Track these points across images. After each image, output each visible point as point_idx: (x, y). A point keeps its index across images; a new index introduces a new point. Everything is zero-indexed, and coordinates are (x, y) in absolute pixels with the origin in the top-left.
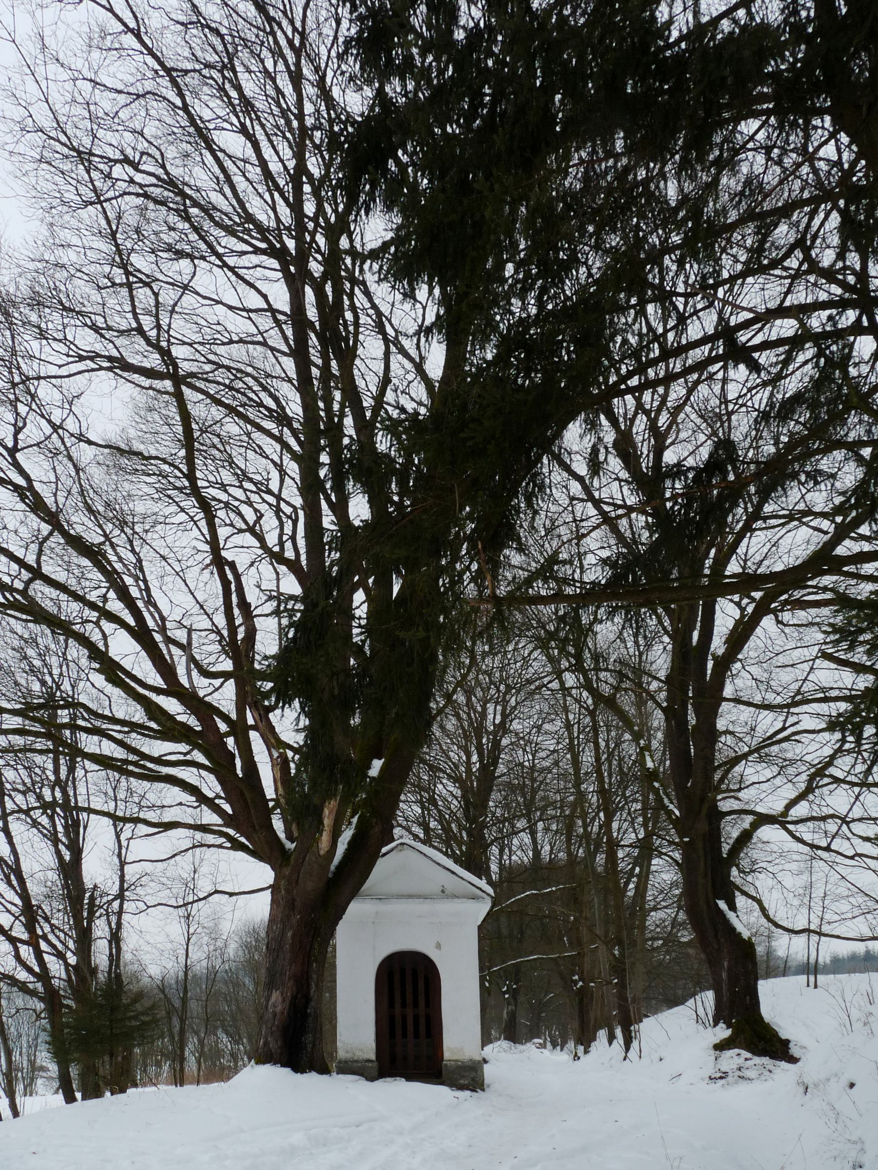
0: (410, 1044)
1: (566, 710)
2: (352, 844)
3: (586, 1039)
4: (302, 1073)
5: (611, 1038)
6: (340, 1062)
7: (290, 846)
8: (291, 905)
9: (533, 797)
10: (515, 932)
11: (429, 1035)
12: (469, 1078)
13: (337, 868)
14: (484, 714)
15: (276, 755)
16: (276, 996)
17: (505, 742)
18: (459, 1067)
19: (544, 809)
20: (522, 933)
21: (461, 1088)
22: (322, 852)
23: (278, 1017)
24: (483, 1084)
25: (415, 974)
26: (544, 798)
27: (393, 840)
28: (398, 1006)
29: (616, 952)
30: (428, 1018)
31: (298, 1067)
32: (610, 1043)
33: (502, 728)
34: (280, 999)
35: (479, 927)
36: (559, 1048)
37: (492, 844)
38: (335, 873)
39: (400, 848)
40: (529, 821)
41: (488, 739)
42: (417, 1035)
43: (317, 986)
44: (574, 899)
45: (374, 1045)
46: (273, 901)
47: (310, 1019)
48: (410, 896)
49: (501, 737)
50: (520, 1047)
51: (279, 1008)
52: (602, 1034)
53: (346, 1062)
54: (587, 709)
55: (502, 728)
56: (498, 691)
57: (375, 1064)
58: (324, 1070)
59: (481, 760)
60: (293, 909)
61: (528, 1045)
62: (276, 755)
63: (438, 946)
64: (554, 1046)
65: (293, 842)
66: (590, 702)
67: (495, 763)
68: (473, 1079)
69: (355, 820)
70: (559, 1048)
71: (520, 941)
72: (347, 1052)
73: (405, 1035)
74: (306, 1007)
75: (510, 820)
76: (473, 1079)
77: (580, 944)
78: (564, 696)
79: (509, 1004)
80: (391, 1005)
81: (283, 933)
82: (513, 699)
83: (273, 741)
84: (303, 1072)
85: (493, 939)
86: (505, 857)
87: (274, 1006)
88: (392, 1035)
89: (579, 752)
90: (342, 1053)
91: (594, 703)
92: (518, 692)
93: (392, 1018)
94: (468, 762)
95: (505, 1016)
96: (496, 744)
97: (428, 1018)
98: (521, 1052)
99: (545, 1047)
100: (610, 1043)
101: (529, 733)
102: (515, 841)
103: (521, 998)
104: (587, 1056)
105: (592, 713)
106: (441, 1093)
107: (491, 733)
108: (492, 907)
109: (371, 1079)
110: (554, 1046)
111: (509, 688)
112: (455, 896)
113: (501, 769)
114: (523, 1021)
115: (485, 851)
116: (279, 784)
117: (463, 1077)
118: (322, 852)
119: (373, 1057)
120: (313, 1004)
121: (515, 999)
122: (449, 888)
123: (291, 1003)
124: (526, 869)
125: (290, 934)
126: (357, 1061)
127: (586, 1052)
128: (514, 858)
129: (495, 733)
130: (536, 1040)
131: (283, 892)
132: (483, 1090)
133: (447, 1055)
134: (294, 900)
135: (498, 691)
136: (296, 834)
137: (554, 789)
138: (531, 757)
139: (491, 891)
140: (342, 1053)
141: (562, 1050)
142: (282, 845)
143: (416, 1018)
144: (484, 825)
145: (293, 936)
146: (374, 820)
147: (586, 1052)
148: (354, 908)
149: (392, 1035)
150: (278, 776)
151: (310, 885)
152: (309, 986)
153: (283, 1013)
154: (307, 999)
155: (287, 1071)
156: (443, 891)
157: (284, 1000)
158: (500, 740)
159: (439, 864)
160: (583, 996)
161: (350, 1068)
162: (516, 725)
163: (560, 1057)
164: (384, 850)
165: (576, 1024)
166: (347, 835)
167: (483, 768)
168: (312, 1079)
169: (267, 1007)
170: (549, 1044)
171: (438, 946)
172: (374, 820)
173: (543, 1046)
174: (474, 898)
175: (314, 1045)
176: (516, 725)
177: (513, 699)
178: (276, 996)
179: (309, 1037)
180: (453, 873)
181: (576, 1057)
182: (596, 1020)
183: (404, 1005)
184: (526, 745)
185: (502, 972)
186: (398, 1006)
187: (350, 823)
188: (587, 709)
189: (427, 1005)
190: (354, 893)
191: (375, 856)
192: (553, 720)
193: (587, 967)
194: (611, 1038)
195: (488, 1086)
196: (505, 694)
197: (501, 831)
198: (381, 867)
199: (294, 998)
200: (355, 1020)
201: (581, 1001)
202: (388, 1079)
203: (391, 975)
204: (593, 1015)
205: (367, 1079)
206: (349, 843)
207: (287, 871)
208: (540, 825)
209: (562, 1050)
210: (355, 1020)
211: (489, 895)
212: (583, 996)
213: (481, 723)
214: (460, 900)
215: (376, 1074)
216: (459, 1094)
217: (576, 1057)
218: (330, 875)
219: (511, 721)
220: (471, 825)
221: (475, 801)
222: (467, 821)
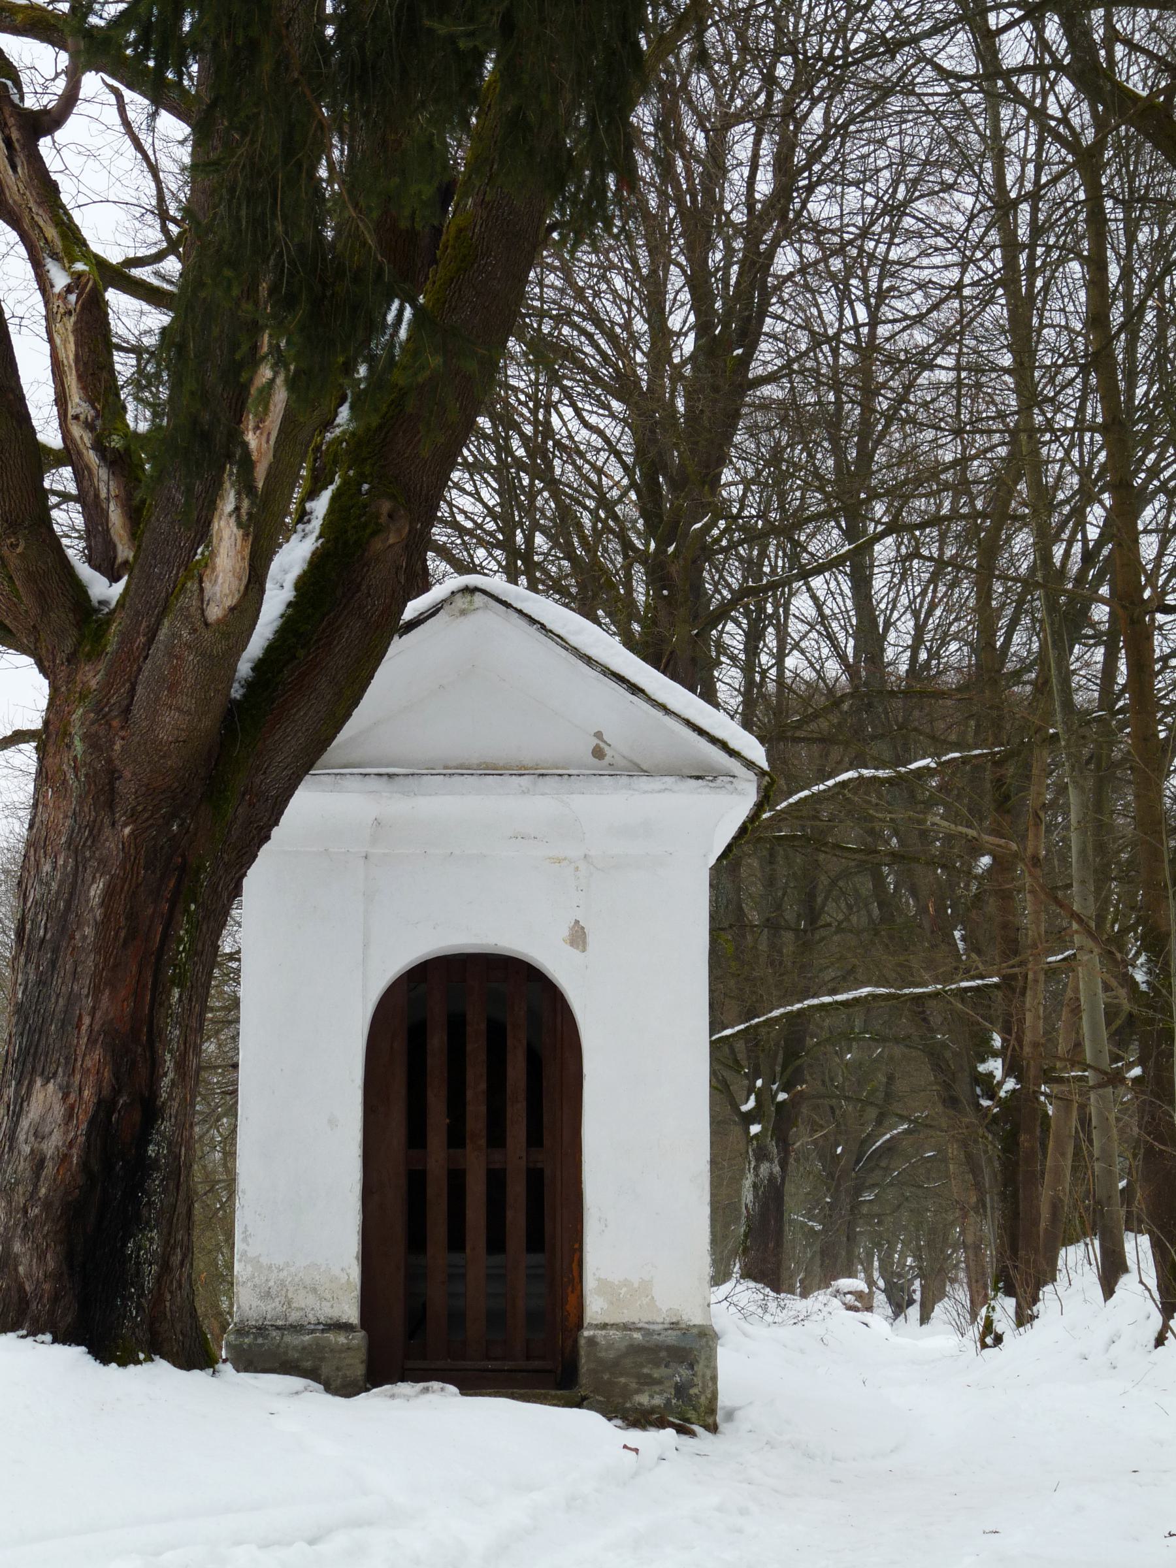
0: (474, 1277)
1: (997, 149)
2: (310, 585)
3: (1021, 1275)
4: (123, 1363)
5: (1112, 1270)
6: (241, 1332)
7: (104, 590)
8: (104, 790)
9: (866, 457)
10: (790, 914)
11: (536, 1241)
12: (665, 1386)
13: (259, 666)
14: (716, 162)
15: (60, 280)
16: (44, 1100)
17: (785, 260)
18: (636, 1350)
19: (899, 494)
20: (813, 915)
21: (640, 1419)
22: (214, 612)
23: (49, 1168)
24: (712, 1411)
25: (496, 1035)
26: (905, 457)
27: (426, 588)
28: (437, 1140)
29: (1140, 976)
30: (536, 1179)
31: (110, 1348)
32: (1108, 1290)
33: (779, 215)
34: (58, 1111)
35: (717, 871)
36: (914, 1312)
37: (723, 614)
38: (250, 686)
39: (460, 602)
40: (849, 534)
41: (729, 251)
42: (496, 1243)
43: (181, 1066)
44: (1000, 796)
45: (354, 1272)
46: (43, 776)
47: (156, 1181)
48: (490, 769)
49: (775, 244)
50: (796, 1304)
51: (53, 1144)
52: (1078, 1262)
53: (261, 1330)
54: (1072, 144)
55: (779, 215)
56: (770, 80)
57: (358, 1338)
58: (194, 1355)
59: (702, 329)
60: (111, 805)
61: (819, 1299)
62: (60, 280)
63: (578, 937)
64: (899, 1306)
65: (114, 578)
66: (1081, 116)
67: (750, 336)
68: (681, 1390)
69: (320, 506)
70: (914, 1312)
71: (806, 946)
72: (267, 1295)
73: (457, 1242)
74: (143, 1140)
75: (788, 528)
76: (681, 1390)
77: (1012, 946)
78: (993, 101)
79: (762, 1155)
80: (417, 1136)
81: (73, 889)
82: (818, 114)
83: (51, 232)
84: (126, 1359)
85: (762, 914)
86: (764, 659)
87: (39, 1135)
88: (416, 1241)
89: (1031, 297)
90: (248, 1301)
91: (1099, 123)
92: (837, 87)
93: (416, 1181)
94: (661, 335)
95: (748, 1196)
96: (757, 264)
97: (536, 1179)
98: (799, 1320)
99: (869, 1308)
100: (1108, 1290)
101: (864, 233)
102: (802, 604)
103: (802, 1140)
104: (1031, 1333)
105: (1088, 162)
106: (572, 1435)
107: (738, 230)
108: (759, 807)
109: (345, 1388)
110: (899, 1306)
111: (803, 82)
112: (637, 770)
113: (766, 357)
114: (800, 1217)
115: (703, 635)
116: (72, 381)
117: (648, 1382)
118: (214, 612)
119: (350, 1312)
120: (165, 1126)
121: (784, 1143)
122: (619, 745)
123: (92, 1122)
124: (834, 699)
125: (96, 891)
126: (297, 1328)
127: (1023, 1319)
128: (792, 661)
129: (752, 233)
130: (845, 1283)
131: (79, 746)
132: (713, 1429)
133: (597, 1307)
134: (113, 774)
135: (770, 80)
136: (124, 552)
137: (940, 431)
138: (862, 315)
139: (757, 752)
140: (248, 1301)
141: (924, 1319)
142: (79, 589)
143: (496, 1180)
144: (705, 552)
145: (109, 894)
146: (386, 506)
147: (1023, 1319)
148: (311, 806)
149: (416, 1241)
150: (69, 353)
151: (172, 721)
152: (154, 1064)
153: (65, 1158)
154: (150, 1111)
155: (76, 1354)
156: (598, 753)
157: (70, 1115)
158: (770, 255)
159: (588, 660)
160: (1017, 1123)
161: (273, 1351)
162: (820, 207)
163: (942, 1337)
164: (412, 609)
165: (988, 1229)
166: (293, 557)
167: (710, 348)
168: (157, 1377)
169: (12, 1136)
170: (880, 1298)
171: (578, 937)
172: (386, 506)
173: (863, 1302)
174: (701, 775)
175: (166, 1268)
176: (820, 207)
177: (818, 114)
178: (44, 1100)
179: (152, 1241)
180: (635, 689)
181: (990, 1337)
182: (1055, 1207)
183: (456, 1138)
184: (849, 271)
185: (740, 1046)
186: (437, 1140)
187: (303, 516)
188: (1072, 144)
189: (535, 1138)
190: (308, 757)
191: (387, 626)
192: (948, 187)
193: (1033, 1025)
194: (1112, 1270)
195: (730, 1416)
196: (790, 94)
197: (751, 567)
198: (403, 666)
199: (104, 1106)
200: (295, 1188)
201: (1010, 1143)
202: (404, 1388)
203: (417, 1035)
204: (1055, 1185)
205: (329, 1389)
206: (302, 584)
207: (92, 677)
208: (885, 550)
209: (924, 1319)
210: (295, 1188)
211: (749, 764)
212: (1017, 1123)
213: (708, 192)
214: (656, 783)
215: (359, 1370)
216: (635, 1436)
217: (990, 1337)
218: (236, 692)
219: (810, 189)
220: (662, 544)
221: (677, 458)
222: (651, 531)
